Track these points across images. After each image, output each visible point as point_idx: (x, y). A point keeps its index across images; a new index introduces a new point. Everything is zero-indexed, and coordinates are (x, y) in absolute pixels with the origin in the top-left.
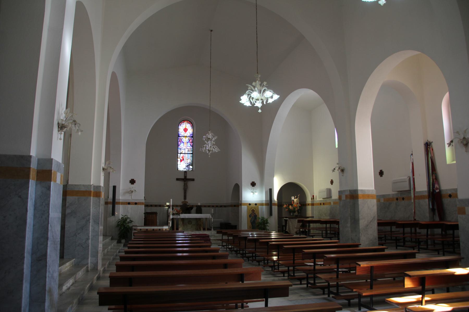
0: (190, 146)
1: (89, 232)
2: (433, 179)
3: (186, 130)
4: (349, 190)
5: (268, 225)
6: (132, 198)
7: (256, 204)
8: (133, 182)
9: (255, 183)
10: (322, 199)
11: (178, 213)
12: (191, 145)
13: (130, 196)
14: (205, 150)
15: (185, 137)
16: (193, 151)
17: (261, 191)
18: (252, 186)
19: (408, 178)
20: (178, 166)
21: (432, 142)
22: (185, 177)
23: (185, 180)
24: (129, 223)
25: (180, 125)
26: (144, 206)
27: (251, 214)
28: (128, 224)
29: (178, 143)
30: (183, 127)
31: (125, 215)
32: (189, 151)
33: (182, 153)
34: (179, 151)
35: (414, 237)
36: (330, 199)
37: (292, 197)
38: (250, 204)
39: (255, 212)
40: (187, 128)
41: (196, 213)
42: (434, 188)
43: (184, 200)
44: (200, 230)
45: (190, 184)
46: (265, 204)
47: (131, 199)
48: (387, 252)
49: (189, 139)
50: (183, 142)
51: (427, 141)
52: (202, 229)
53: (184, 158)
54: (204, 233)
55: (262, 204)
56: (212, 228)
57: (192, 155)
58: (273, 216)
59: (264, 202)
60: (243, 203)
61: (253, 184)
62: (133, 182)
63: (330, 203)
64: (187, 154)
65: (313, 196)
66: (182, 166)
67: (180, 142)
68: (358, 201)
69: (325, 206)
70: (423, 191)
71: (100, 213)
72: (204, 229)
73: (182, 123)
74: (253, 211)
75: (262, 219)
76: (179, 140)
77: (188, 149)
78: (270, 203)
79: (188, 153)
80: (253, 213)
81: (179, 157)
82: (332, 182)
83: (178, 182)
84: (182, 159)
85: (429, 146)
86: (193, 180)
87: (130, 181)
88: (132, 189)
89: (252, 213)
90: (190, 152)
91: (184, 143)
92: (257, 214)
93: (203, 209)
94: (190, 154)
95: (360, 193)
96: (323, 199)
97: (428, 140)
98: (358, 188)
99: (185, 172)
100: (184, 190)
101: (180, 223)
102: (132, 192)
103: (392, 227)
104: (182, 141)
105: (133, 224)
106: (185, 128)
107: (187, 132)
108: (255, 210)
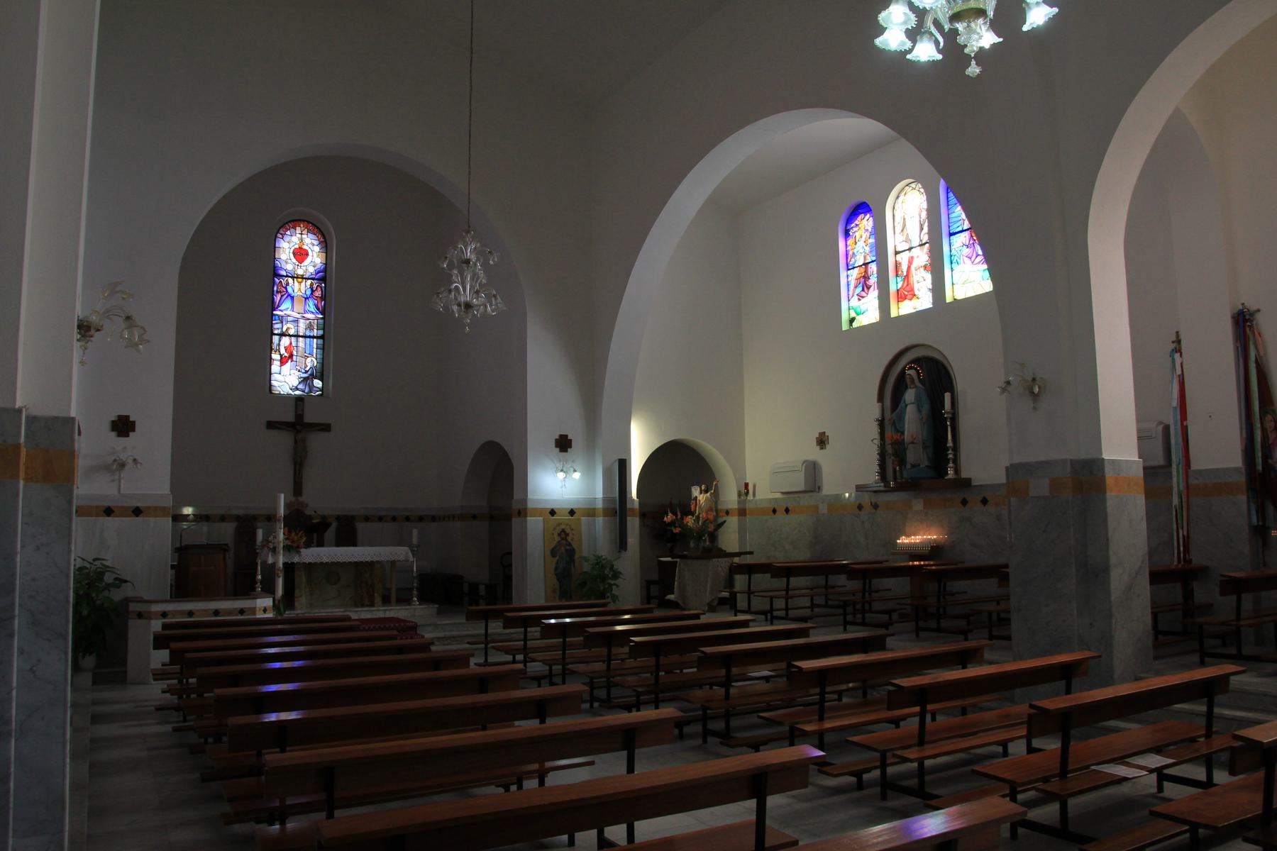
0: (313, 309)
1: (10, 692)
2: (1264, 430)
3: (300, 254)
4: (1071, 460)
5: (619, 581)
6: (122, 492)
7: (572, 512)
8: (123, 426)
9: (571, 440)
10: (779, 496)
11: (295, 545)
12: (318, 309)
13: (113, 481)
14: (446, 308)
15: (297, 278)
16: (324, 329)
17: (589, 471)
18: (561, 451)
19: (1160, 428)
20: (273, 378)
21: (1258, 311)
22: (299, 417)
23: (298, 427)
24: (111, 589)
25: (281, 236)
26: (171, 519)
27: (555, 547)
28: (106, 593)
29: (273, 298)
30: (292, 245)
31: (94, 560)
32: (310, 327)
33: (285, 335)
34: (277, 327)
35: (1235, 623)
36: (815, 494)
37: (693, 490)
38: (553, 512)
39: (569, 539)
40: (305, 247)
41: (338, 545)
42: (1270, 461)
43: (293, 499)
44: (372, 605)
45: (316, 441)
46: (604, 509)
47: (116, 493)
48: (817, 637)
49: (312, 285)
50: (289, 295)
51: (1241, 307)
52: (378, 599)
53: (295, 353)
54: (388, 615)
55: (591, 512)
56: (412, 598)
57: (320, 341)
58: (627, 552)
59: (600, 505)
60: (535, 509)
61: (563, 444)
62: (123, 426)
63: (816, 507)
64: (305, 337)
65: (747, 485)
66: (286, 379)
67: (279, 296)
68: (1104, 501)
69: (793, 518)
70: (1224, 470)
71: (68, 576)
72: (386, 601)
73: (287, 230)
74: (563, 536)
75: (597, 564)
76: (275, 288)
77: (308, 322)
78: (618, 507)
79: (308, 334)
80: (564, 542)
81: (274, 346)
82: (822, 441)
83: (275, 435)
84: (286, 355)
85: (1248, 324)
86: (326, 428)
87: (113, 422)
88: (123, 457)
89: (559, 542)
90: (315, 331)
91: (292, 298)
92: (574, 546)
93: (361, 527)
94: (314, 337)
95: (1109, 473)
96: (785, 496)
97: (1243, 304)
98: (1101, 453)
99: (299, 399)
100: (295, 464)
101: (301, 578)
102: (123, 465)
103: (1244, 596)
104: (287, 291)
105: (127, 591)
106: (297, 246)
107: (307, 262)
108: (568, 531)
